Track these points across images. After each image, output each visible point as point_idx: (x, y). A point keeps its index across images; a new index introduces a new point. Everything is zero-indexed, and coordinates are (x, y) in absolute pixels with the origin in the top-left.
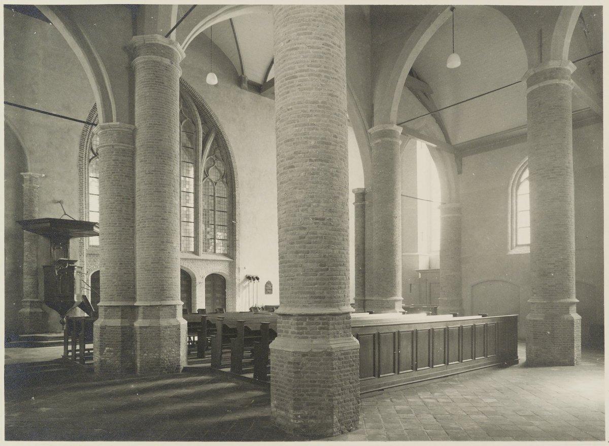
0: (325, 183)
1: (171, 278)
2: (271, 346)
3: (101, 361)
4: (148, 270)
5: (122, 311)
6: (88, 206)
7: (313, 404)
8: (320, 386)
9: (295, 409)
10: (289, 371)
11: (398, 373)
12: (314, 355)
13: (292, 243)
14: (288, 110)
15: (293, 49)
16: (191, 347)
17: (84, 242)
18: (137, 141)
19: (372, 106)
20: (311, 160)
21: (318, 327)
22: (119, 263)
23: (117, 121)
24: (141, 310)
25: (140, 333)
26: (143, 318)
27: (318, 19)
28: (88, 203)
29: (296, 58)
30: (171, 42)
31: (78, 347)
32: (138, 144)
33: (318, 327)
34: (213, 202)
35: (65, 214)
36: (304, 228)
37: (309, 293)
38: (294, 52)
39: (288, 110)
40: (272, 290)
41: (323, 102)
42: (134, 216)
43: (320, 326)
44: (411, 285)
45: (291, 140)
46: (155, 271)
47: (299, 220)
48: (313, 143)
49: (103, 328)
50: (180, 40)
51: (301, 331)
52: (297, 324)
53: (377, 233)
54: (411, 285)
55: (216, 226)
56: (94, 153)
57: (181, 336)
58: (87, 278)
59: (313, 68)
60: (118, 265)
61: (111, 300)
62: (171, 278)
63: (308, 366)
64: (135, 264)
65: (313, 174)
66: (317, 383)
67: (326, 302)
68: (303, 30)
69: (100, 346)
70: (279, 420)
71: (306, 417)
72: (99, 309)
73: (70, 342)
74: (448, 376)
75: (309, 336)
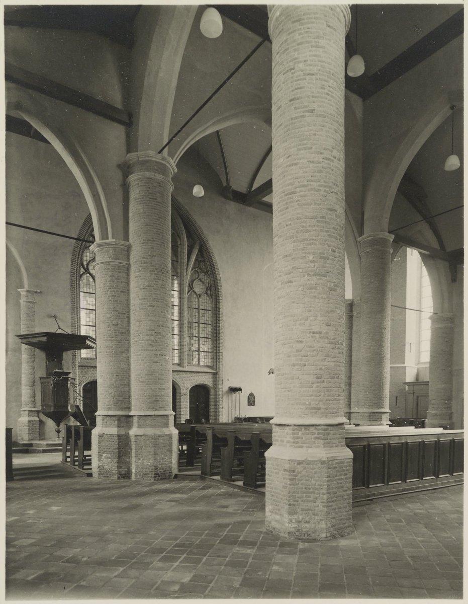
0: (322, 298)
1: (164, 389)
2: (266, 454)
3: (324, 447)
4: (142, 382)
5: (118, 420)
6: (80, 320)
7: (309, 509)
8: (314, 493)
9: (290, 513)
10: (284, 478)
11: (388, 485)
12: (309, 463)
13: (289, 356)
14: (287, 225)
15: (293, 165)
16: (181, 454)
17: (77, 355)
18: (131, 257)
19: (363, 214)
20: (309, 275)
21: (313, 437)
22: (115, 375)
23: (113, 238)
24: (135, 420)
25: (135, 442)
26: (138, 427)
27: (318, 133)
28: (80, 318)
29: (296, 173)
30: (164, 159)
31: (77, 454)
32: (132, 261)
33: (313, 437)
34: (197, 314)
35: (59, 328)
36: (301, 342)
37: (304, 404)
38: (294, 167)
39: (287, 225)
40: (254, 401)
41: (323, 217)
42: (128, 330)
43: (316, 436)
44: (397, 397)
45: (290, 255)
46: (149, 383)
47: (296, 334)
48: (311, 257)
49: (101, 436)
50: (171, 155)
51: (296, 440)
52: (293, 434)
53: (365, 345)
54: (397, 397)
55: (201, 339)
56: (84, 268)
57: (173, 445)
58: (79, 389)
59: (312, 183)
60: (115, 376)
61: (109, 409)
62: (164, 389)
63: (304, 473)
64: (130, 376)
65: (311, 289)
66: (311, 490)
67: (322, 413)
68: (303, 145)
69: (99, 452)
70: (274, 524)
71: (300, 522)
72: (97, 419)
73: (69, 449)
74: (437, 489)
75: (305, 445)
